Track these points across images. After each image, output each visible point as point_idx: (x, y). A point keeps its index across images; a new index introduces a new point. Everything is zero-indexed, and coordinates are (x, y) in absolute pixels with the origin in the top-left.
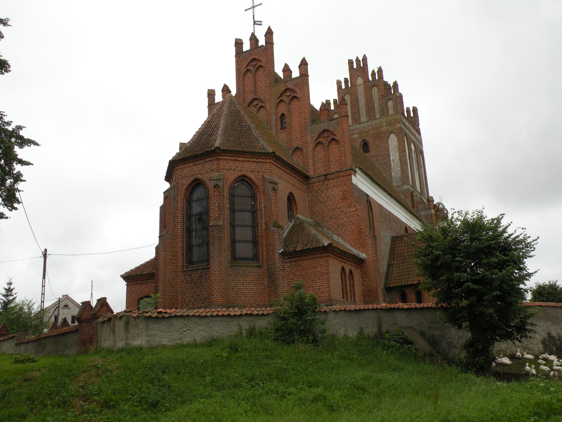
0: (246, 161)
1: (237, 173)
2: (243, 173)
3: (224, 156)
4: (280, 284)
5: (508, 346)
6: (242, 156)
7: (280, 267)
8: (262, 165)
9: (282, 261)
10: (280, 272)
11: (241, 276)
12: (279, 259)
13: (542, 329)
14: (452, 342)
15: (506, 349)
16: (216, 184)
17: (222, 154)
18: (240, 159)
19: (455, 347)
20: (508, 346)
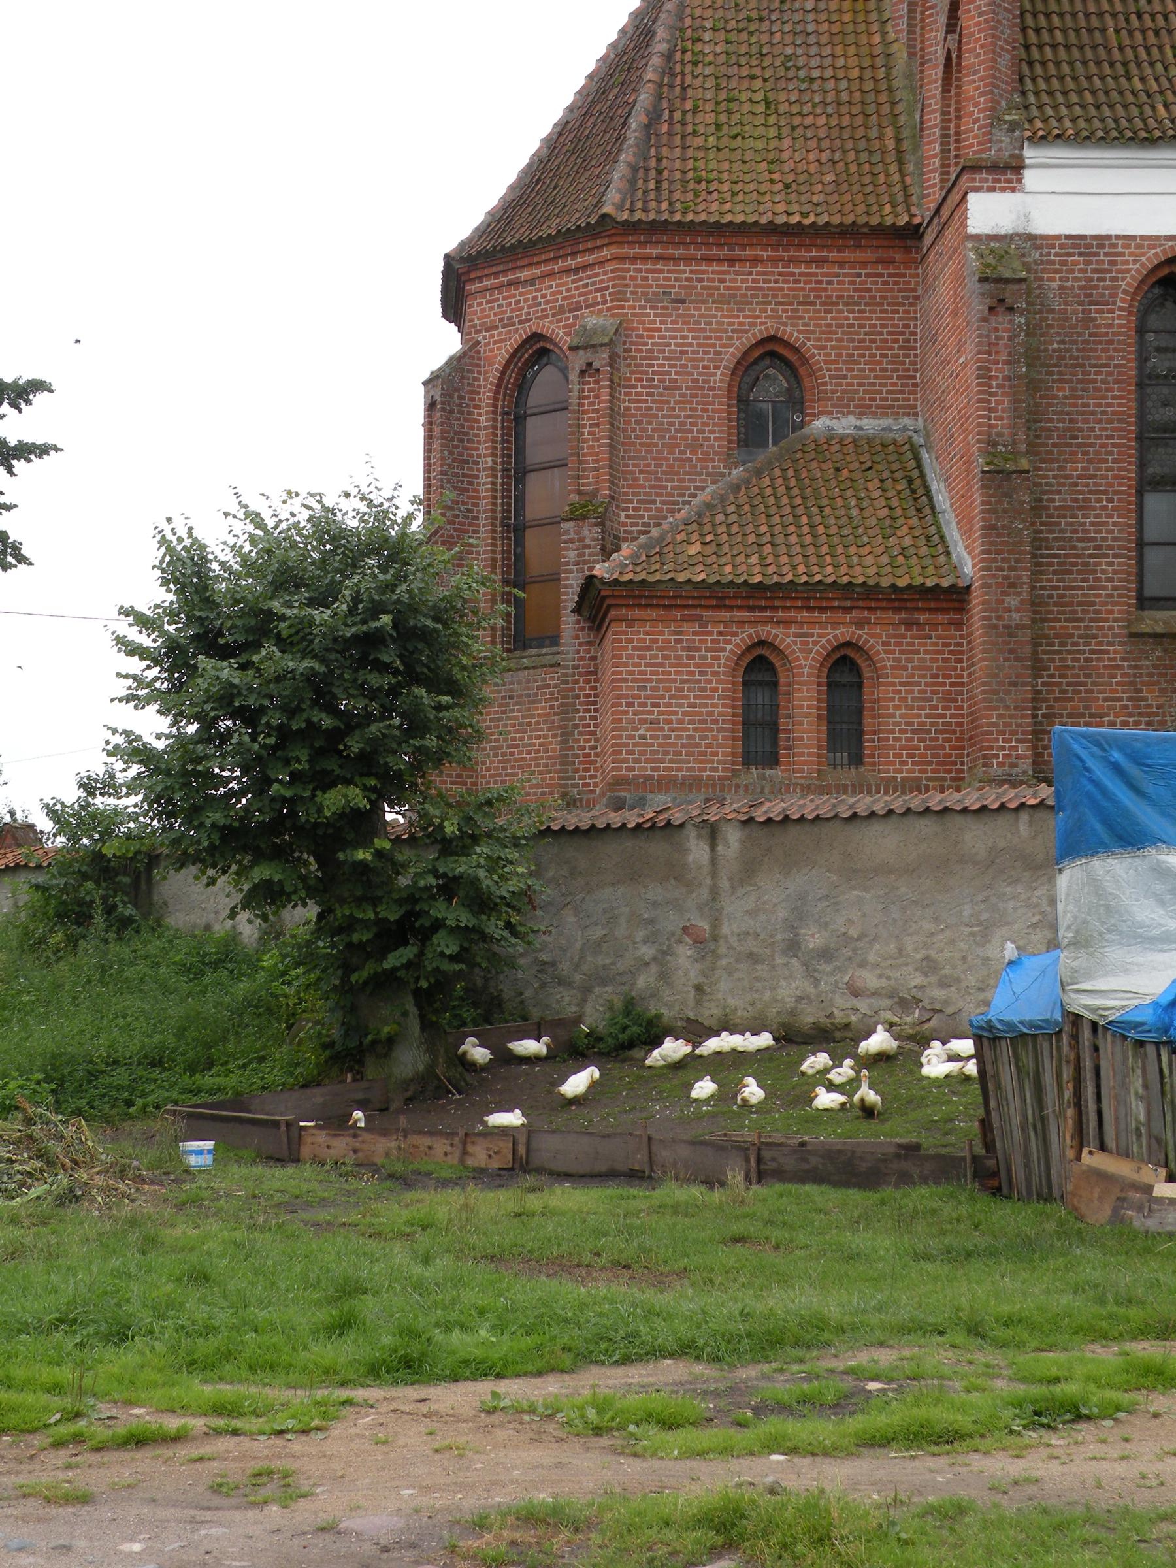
0: (544, 276)
1: (516, 331)
2: (535, 326)
3: (480, 279)
4: (576, 726)
5: (811, 990)
6: (526, 261)
7: (578, 667)
8: (589, 277)
9: (589, 643)
10: (577, 682)
11: (517, 704)
12: (577, 637)
13: (1037, 918)
14: (553, 964)
15: (799, 999)
16: (589, 364)
17: (473, 275)
18: (524, 275)
19: (561, 982)
20: (811, 990)
